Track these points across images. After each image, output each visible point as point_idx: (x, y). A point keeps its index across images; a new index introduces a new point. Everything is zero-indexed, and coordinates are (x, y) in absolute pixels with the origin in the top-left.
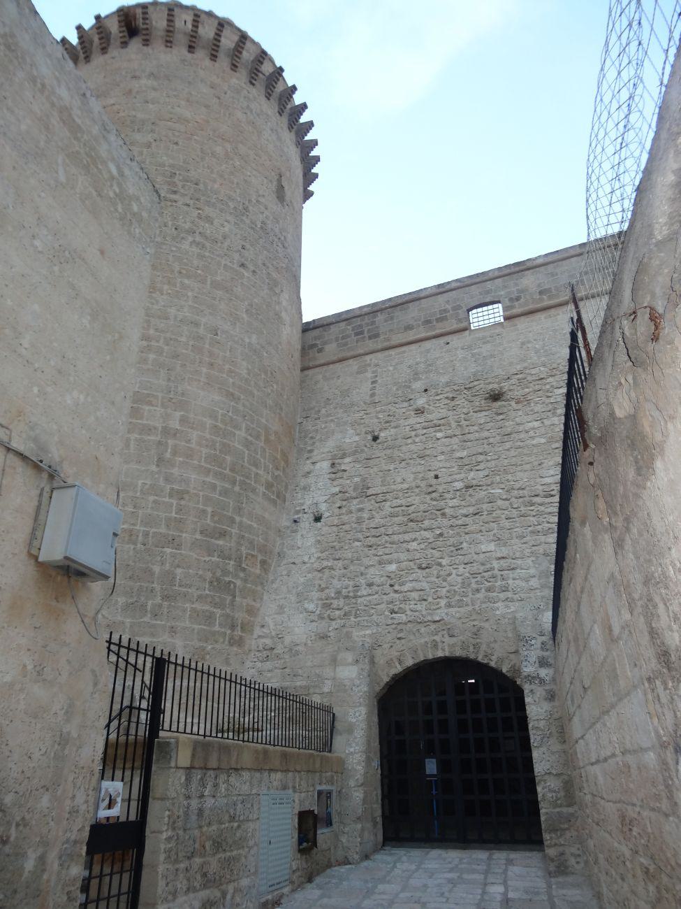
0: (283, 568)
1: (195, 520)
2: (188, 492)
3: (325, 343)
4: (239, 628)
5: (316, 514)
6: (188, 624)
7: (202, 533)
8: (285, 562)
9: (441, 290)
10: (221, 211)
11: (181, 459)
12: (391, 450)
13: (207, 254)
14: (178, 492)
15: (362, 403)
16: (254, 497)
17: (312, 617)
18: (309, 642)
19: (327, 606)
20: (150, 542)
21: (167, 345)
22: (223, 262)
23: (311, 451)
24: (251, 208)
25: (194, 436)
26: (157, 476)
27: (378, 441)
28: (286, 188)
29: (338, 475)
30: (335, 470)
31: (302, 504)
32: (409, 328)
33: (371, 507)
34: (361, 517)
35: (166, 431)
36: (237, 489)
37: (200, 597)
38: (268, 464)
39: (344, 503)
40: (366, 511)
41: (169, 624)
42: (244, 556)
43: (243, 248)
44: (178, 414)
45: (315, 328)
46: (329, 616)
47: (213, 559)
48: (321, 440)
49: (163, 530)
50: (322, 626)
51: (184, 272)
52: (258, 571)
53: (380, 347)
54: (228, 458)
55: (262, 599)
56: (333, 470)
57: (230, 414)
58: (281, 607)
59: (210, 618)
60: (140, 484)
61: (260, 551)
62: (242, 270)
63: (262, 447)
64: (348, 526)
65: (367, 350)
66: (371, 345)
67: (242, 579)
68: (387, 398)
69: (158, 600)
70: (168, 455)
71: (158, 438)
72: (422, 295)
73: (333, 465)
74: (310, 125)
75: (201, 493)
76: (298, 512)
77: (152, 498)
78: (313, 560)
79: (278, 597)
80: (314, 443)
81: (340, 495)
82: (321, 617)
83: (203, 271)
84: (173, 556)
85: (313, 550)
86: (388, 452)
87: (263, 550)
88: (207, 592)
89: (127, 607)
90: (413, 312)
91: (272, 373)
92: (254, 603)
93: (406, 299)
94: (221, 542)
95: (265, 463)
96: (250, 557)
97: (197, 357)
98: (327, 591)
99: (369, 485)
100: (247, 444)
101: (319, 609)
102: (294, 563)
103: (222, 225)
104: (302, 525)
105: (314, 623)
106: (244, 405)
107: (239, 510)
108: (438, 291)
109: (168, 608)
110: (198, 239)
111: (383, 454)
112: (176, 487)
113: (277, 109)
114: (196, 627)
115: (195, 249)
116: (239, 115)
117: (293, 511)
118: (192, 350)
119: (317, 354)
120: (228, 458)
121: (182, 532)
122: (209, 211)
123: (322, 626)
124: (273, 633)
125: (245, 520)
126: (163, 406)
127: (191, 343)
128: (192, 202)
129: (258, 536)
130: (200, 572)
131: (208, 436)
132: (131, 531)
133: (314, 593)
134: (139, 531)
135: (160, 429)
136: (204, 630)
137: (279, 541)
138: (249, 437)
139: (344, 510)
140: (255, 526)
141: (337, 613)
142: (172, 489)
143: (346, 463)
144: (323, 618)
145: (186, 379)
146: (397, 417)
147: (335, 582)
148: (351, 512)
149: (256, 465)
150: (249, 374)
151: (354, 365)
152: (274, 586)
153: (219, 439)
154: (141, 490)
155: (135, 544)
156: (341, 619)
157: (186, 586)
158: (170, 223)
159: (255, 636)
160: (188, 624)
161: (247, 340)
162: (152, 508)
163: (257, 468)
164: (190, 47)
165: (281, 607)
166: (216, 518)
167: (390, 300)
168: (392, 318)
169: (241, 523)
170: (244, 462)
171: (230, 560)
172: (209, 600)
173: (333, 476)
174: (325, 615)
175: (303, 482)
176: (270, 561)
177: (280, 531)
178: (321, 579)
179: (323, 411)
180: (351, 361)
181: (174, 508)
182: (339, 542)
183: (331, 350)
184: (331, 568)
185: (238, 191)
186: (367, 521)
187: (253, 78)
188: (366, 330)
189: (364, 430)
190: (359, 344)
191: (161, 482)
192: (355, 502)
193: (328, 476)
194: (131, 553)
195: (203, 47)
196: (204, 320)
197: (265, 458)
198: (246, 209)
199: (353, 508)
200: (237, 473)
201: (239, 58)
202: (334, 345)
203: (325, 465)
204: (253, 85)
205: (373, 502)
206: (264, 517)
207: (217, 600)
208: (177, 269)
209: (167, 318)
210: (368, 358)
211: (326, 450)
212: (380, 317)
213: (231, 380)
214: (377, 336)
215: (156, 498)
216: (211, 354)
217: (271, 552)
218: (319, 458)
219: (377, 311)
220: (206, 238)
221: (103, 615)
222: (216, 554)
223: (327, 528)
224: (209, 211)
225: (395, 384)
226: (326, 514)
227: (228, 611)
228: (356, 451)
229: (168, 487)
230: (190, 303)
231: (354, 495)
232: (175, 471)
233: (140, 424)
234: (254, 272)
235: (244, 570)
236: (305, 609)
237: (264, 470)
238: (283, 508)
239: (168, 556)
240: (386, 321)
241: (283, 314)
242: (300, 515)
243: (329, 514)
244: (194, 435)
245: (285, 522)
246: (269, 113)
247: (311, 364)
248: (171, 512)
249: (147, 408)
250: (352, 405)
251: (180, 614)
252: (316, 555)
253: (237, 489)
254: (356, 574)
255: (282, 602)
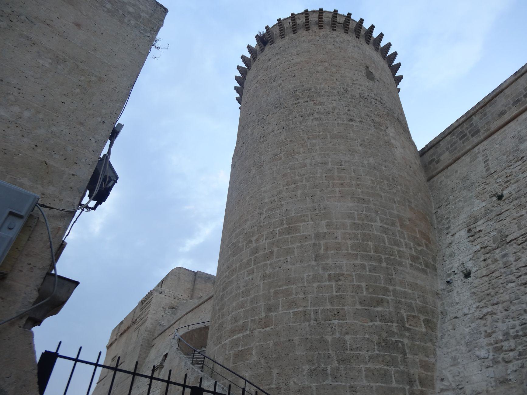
0: (448, 323)
1: (352, 294)
2: (343, 275)
3: (441, 155)
4: (417, 383)
5: (465, 271)
6: (365, 382)
7: (361, 303)
8: (448, 318)
9: (518, 75)
10: (328, 96)
11: (332, 252)
12: (518, 200)
13: (324, 122)
14: (334, 276)
15: (480, 179)
16: (401, 269)
17: (487, 363)
18: (490, 389)
19: (499, 350)
20: (320, 317)
21: (308, 181)
22: (336, 122)
23: (448, 228)
24: (349, 89)
25: (339, 233)
26: (316, 268)
27: (503, 199)
28: (374, 72)
29: (476, 237)
30: (472, 234)
31: (451, 268)
32: (502, 113)
33: (515, 250)
34: (508, 262)
35: (318, 236)
36: (384, 265)
37: (371, 358)
38: (408, 242)
39: (488, 255)
40: (511, 255)
41: (348, 384)
42: (405, 317)
43: (348, 110)
44: (324, 222)
45: (431, 148)
46: (503, 359)
47: (376, 324)
48: (454, 217)
49: (329, 307)
50: (499, 371)
51: (311, 137)
52: (424, 330)
53: (482, 137)
54: (371, 244)
55: (435, 354)
56: (470, 234)
57: (364, 212)
58: (454, 359)
59: (384, 376)
60: (305, 277)
61: (420, 311)
62: (351, 123)
63: (399, 231)
64: (497, 272)
65: (474, 144)
66: (475, 140)
67: (408, 338)
68: (500, 166)
69: (335, 364)
70: (322, 251)
71: (313, 242)
72: (503, 87)
73: (469, 231)
74: (381, 36)
75: (354, 273)
76: (449, 275)
77: (315, 285)
78: (473, 310)
79: (450, 350)
80: (449, 222)
81: (482, 250)
82: (496, 362)
83: (323, 132)
84: (341, 325)
85: (471, 302)
86: (515, 202)
87: (423, 310)
88: (377, 352)
89: (311, 372)
90: (501, 101)
91: (393, 179)
92: (427, 359)
93: (492, 95)
94: (380, 309)
95: (406, 242)
96: (411, 318)
97: (330, 182)
98: (494, 335)
99: (506, 233)
100: (385, 231)
101: (491, 354)
102: (456, 317)
103: (331, 103)
104: (455, 284)
105: (490, 369)
106: (374, 204)
107: (391, 281)
108: (516, 77)
109: (345, 370)
110: (316, 116)
111: (511, 206)
112: (332, 272)
113: (354, 36)
114: (374, 385)
115: (316, 122)
116: (330, 47)
117: (445, 275)
118: (326, 180)
119: (436, 165)
120: (371, 244)
121: (344, 305)
122: (319, 99)
123: (499, 371)
124: (454, 385)
125: (398, 288)
126: (312, 220)
127: (324, 176)
128: (308, 99)
129: (415, 300)
130: (367, 336)
131: (350, 232)
132: (305, 312)
133: (482, 340)
134: (310, 310)
135: (313, 236)
136: (382, 387)
137: (439, 303)
138: (385, 226)
139: (489, 261)
140: (410, 291)
141: (511, 354)
142: (330, 275)
143: (480, 225)
144: (498, 362)
145: (326, 198)
146: (514, 174)
147: (500, 324)
148: (496, 260)
149: (397, 244)
150: (373, 183)
151: (466, 159)
152: (444, 341)
153: (359, 231)
154: (307, 280)
155: (309, 321)
156: (518, 360)
157: (357, 349)
158: (298, 115)
159: (437, 390)
160: (365, 382)
161: (366, 162)
162: (317, 292)
163: (398, 246)
164: (294, 31)
165: (454, 359)
166: (371, 290)
167: (479, 103)
168: (485, 115)
169: (394, 291)
170: (385, 244)
171: (392, 322)
172: (381, 359)
173: (472, 238)
174: (500, 359)
175: (448, 252)
176: (435, 320)
177: (437, 294)
178: (485, 325)
179: (451, 197)
180: (463, 158)
181: (334, 288)
182: (493, 289)
183: (446, 158)
184: (492, 313)
185: (338, 83)
186: (514, 263)
187: (333, 27)
188: (467, 132)
189: (488, 196)
190: (465, 144)
191: (321, 272)
192: (497, 251)
193: (468, 240)
194: (308, 328)
195: (302, 28)
196: (330, 159)
197: (404, 238)
198: (346, 90)
199: (498, 257)
200: (380, 253)
201: (322, 21)
202: (447, 153)
203: (463, 233)
204: (335, 30)
205: (515, 245)
206: (417, 284)
207: (389, 359)
208: (306, 136)
209: (305, 166)
210: (476, 149)
211: (461, 222)
212: (475, 119)
213: (359, 190)
214: (478, 131)
215: (319, 283)
216: (340, 178)
217: (433, 312)
218: (456, 230)
219: (471, 116)
220: (322, 114)
221: (294, 382)
222: (378, 319)
223: (478, 280)
224: (319, 99)
225: (504, 154)
226: (474, 269)
227: (402, 368)
228: (486, 213)
229: (327, 274)
230: (319, 152)
231: (495, 246)
232: (330, 261)
233: (298, 236)
234: (360, 121)
235: (409, 330)
236: (478, 356)
237: (406, 247)
238: (436, 275)
239: (337, 326)
240: (481, 119)
241: (393, 141)
242: (452, 277)
243: (476, 269)
244: (339, 233)
245: (440, 285)
246: (350, 39)
247: (434, 173)
248: (332, 292)
249: (301, 224)
250: (473, 184)
251: (357, 374)
252: (474, 306)
253: (384, 265)
254: (518, 312)
255: (454, 354)
